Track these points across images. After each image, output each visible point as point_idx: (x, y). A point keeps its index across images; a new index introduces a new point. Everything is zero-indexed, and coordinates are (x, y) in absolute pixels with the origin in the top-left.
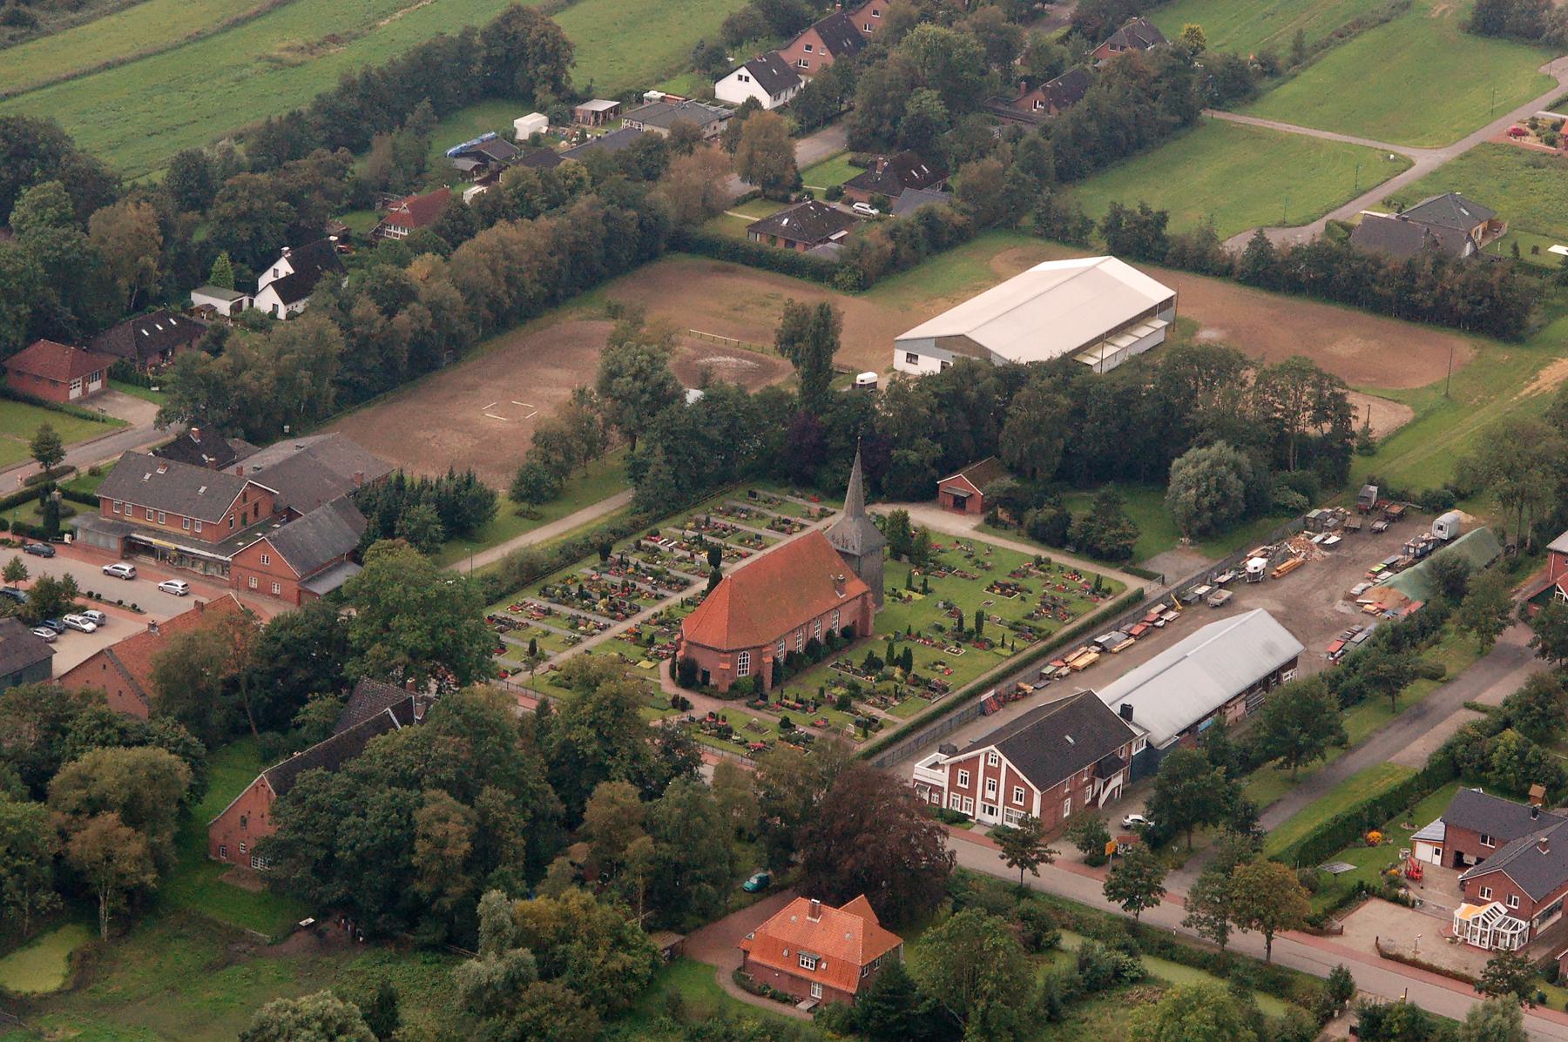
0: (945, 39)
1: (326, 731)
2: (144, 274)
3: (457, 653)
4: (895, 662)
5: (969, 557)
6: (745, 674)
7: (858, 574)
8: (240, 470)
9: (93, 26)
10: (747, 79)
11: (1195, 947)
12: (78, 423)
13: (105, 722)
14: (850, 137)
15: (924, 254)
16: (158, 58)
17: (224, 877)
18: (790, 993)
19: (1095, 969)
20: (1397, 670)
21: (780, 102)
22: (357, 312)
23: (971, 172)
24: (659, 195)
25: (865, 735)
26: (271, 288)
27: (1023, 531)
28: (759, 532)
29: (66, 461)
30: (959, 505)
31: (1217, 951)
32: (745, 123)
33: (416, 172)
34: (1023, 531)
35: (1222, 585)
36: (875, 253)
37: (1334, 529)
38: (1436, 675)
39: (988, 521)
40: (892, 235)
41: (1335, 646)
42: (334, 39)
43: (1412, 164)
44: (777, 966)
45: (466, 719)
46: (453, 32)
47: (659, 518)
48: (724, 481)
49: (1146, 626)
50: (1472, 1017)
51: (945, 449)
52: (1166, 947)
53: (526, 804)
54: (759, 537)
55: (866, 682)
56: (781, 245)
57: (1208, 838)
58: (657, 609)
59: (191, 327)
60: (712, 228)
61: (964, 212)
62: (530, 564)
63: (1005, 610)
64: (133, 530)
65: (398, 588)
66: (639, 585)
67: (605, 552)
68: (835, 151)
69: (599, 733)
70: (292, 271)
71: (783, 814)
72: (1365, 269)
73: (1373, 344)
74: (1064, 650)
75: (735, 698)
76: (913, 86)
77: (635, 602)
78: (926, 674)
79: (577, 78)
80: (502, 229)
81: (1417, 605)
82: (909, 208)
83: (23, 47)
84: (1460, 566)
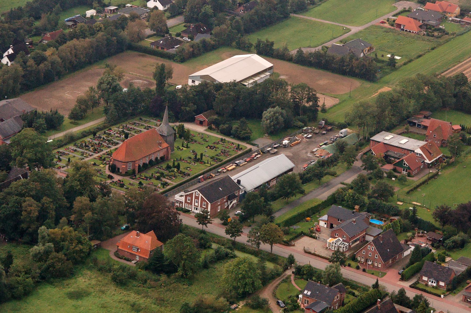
3: (43, 159)
4: (175, 167)
5: (202, 138)
6: (130, 168)
7: (166, 142)
11: (251, 248)
18: (130, 258)
19: (220, 254)
20: (321, 173)
21: (166, 8)
22: (28, 64)
24: (125, 34)
25: (163, 187)
26: (6, 57)
28: (141, 130)
30: (201, 123)
31: (257, 249)
32: (152, 13)
33: (54, 26)
34: (219, 131)
35: (275, 148)
37: (311, 133)
38: (333, 174)
39: (209, 128)
40: (192, 47)
43: (350, 31)
45: (39, 177)
48: (133, 115)
49: (250, 158)
50: (326, 269)
52: (243, 248)
53: (57, 203)
54: (141, 131)
55: (166, 172)
56: (160, 49)
57: (259, 218)
58: (107, 151)
62: (72, 137)
63: (210, 153)
66: (103, 143)
67: (94, 134)
68: (180, 23)
71: (133, 207)
72: (330, 59)
77: (101, 148)
78: (183, 171)
80: (75, 41)
81: (331, 155)
82: (198, 39)
84: (344, 144)
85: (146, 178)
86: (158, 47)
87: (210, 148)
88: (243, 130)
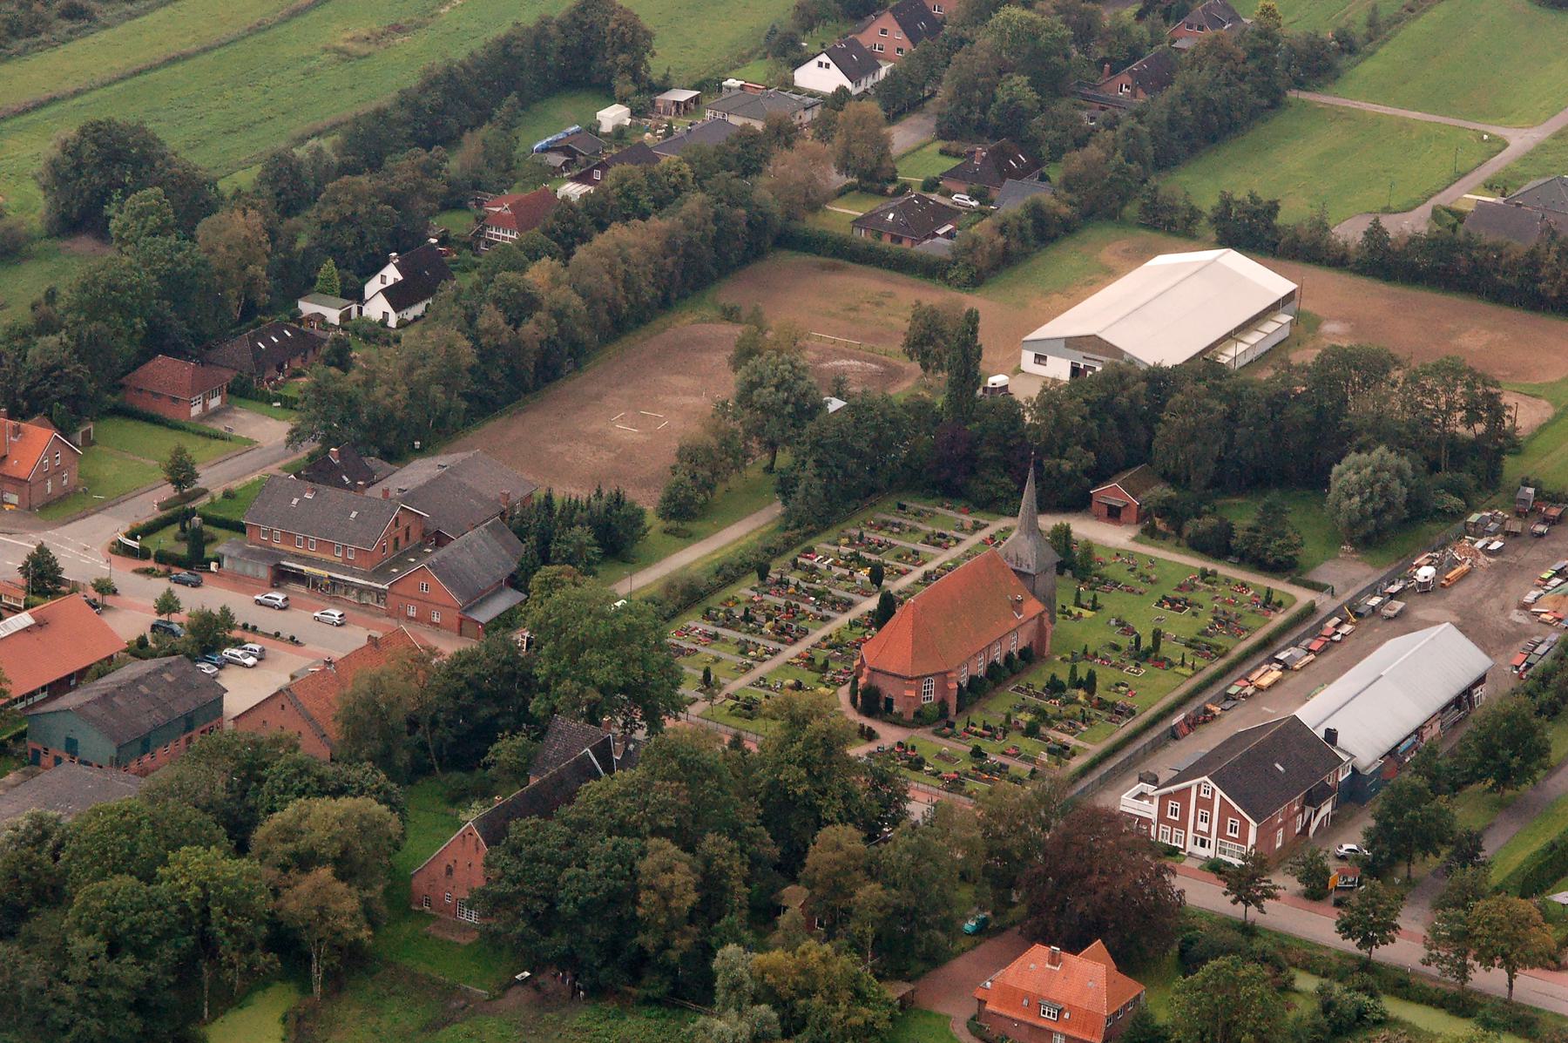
0: (1033, 21)
1: (519, 774)
2: (252, 282)
5: (1132, 570)
6: (929, 701)
8: (386, 492)
9: (149, 19)
10: (827, 66)
12: (201, 441)
13: (303, 770)
14: (938, 125)
15: (1030, 247)
16: (222, 51)
17: (431, 928)
19: (1338, 1014)
22: (483, 322)
23: (1076, 160)
24: (763, 188)
27: (1182, 542)
28: (913, 547)
29: (201, 483)
30: (1114, 515)
33: (503, 168)
35: (1393, 596)
36: (988, 249)
39: (1144, 531)
40: (1002, 230)
41: (1519, 659)
42: (398, 29)
43: (1506, 145)
44: (1016, 1015)
45: (682, 763)
46: (529, 18)
47: (810, 534)
49: (1331, 642)
51: (1098, 459)
52: (1403, 986)
54: (916, 552)
55: (1052, 706)
59: (307, 339)
60: (813, 224)
61: (1071, 203)
63: (1179, 626)
64: (283, 558)
65: (587, 621)
66: (803, 606)
67: (763, 573)
68: (923, 139)
69: (809, 773)
70: (400, 278)
73: (1500, 335)
74: (1246, 668)
75: (921, 725)
76: (1000, 73)
78: (1110, 697)
79: (656, 67)
80: (618, 234)
82: (1013, 201)
83: (83, 41)
85: (990, 732)
86: (879, 236)
87: (1173, 607)
88: (1275, 535)
